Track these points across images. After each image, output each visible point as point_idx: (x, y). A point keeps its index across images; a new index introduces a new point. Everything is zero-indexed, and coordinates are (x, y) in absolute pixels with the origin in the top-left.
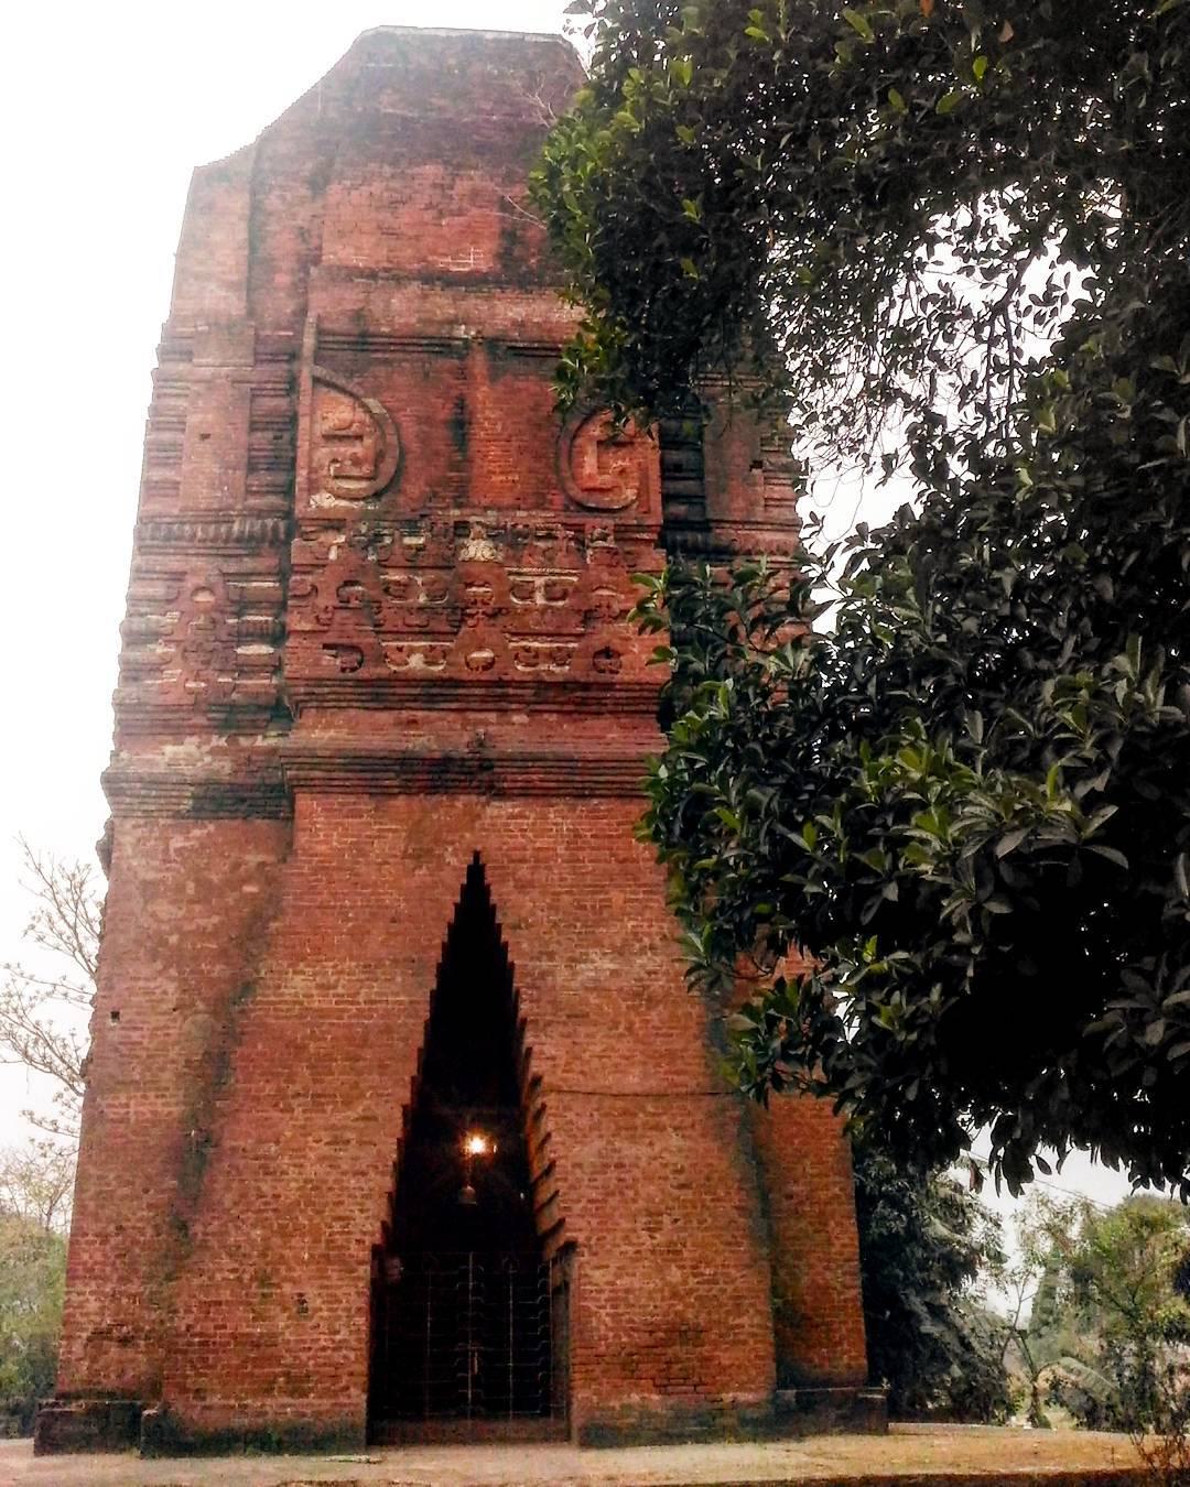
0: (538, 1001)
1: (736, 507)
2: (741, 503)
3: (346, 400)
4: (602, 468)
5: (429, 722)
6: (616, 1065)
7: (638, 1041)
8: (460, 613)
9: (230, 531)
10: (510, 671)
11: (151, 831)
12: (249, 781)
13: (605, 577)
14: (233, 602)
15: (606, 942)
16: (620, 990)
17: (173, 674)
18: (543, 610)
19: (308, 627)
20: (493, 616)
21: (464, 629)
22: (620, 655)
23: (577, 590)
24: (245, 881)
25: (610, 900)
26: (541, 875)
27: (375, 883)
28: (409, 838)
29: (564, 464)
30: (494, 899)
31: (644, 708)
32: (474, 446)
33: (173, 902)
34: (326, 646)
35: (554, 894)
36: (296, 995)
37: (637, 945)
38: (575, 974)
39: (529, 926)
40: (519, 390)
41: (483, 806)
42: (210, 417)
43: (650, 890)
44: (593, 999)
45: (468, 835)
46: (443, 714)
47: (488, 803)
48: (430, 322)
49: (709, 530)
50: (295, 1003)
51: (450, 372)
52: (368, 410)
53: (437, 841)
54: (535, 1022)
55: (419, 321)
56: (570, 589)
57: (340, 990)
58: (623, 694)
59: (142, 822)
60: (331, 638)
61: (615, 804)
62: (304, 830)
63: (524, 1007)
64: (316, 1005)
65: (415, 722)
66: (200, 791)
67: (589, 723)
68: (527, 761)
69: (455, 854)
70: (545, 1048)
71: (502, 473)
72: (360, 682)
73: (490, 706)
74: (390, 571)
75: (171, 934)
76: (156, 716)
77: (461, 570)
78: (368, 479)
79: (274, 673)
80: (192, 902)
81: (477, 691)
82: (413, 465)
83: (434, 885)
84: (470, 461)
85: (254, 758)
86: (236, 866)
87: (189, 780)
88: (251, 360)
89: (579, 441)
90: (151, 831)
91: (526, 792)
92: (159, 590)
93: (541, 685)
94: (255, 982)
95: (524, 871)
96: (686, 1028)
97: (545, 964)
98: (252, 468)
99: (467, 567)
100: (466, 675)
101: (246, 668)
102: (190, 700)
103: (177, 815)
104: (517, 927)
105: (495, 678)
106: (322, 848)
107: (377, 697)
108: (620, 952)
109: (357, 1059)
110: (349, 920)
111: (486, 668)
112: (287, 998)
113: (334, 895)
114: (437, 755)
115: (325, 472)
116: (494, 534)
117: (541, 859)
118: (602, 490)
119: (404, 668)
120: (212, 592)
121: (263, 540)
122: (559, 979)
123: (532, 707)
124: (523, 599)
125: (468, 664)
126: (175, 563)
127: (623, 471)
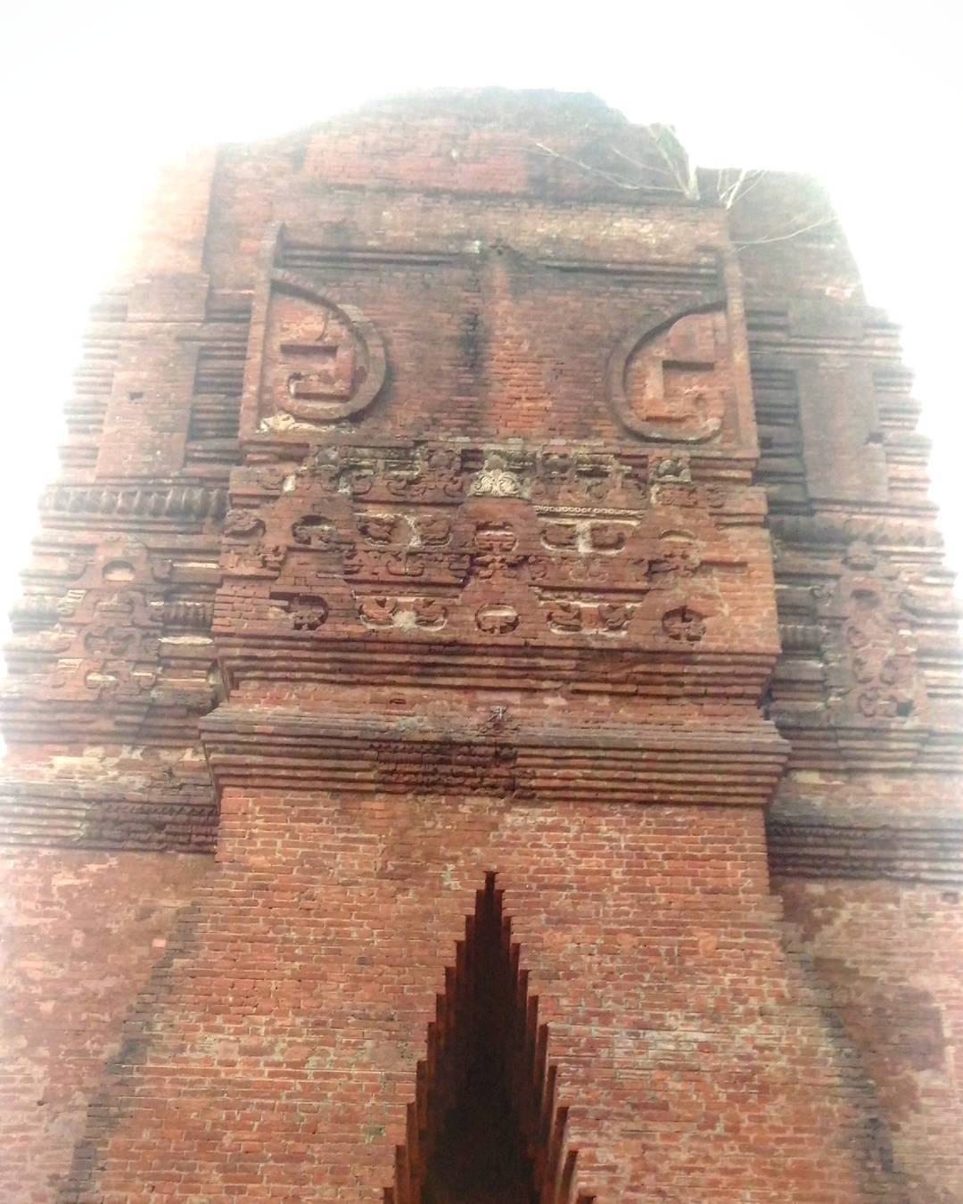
0: (585, 1081)
1: (851, 487)
2: (855, 480)
3: (317, 310)
4: (669, 395)
5: (424, 701)
6: (715, 1183)
7: (746, 1147)
8: (472, 564)
9: (160, 503)
10: (541, 634)
11: (27, 864)
12: (166, 798)
13: (679, 520)
14: (157, 579)
15: (692, 1001)
16: (716, 1070)
17: (73, 662)
18: (590, 559)
19: (249, 570)
20: (512, 566)
21: (473, 581)
22: (701, 617)
23: (636, 535)
24: (158, 933)
25: (695, 944)
26: (587, 907)
27: (337, 909)
28: (389, 851)
29: (616, 387)
30: (516, 937)
31: (738, 690)
32: (493, 368)
33: (51, 958)
34: (274, 596)
35: (608, 932)
36: (207, 1060)
37: (741, 1008)
38: (643, 1046)
39: (570, 975)
40: (555, 306)
41: (502, 811)
42: (144, 375)
43: (753, 930)
44: (675, 1085)
45: (477, 850)
46: (440, 693)
47: (507, 810)
48: (435, 236)
49: (812, 513)
50: (205, 1073)
51: (459, 284)
52: (344, 319)
53: (429, 856)
54: (581, 1114)
55: (419, 234)
56: (628, 534)
57: (277, 1057)
58: (708, 669)
59: (15, 851)
60: (282, 586)
61: (693, 815)
62: (232, 835)
63: (563, 1091)
64: (239, 1076)
65: (400, 702)
66: (98, 811)
67: (657, 708)
68: (561, 750)
69: (458, 874)
70: (599, 1153)
71: (528, 399)
72: (323, 643)
73: (512, 683)
74: (369, 507)
75: (43, 1000)
76: (44, 717)
77: (470, 507)
78: (343, 398)
79: (210, 670)
80: (76, 956)
81: (493, 661)
82: (402, 385)
83: (428, 916)
84: (485, 384)
85: (178, 773)
86: (145, 914)
87: (83, 794)
88: (201, 316)
89: (637, 364)
90: (27, 864)
91: (564, 795)
92: (61, 566)
93: (586, 654)
94: (147, 1041)
95: (562, 901)
96: (825, 1131)
97: (595, 1030)
98: (195, 434)
99: (481, 504)
100: (475, 637)
101: (165, 661)
102: (90, 696)
103: (65, 844)
104: (550, 976)
105: (521, 642)
106: (259, 860)
107: (347, 667)
108: (713, 1016)
109: (298, 1158)
110: (294, 959)
111: (503, 630)
112: (193, 1066)
113: (273, 924)
114: (433, 737)
115: (282, 388)
116: (520, 466)
117: (589, 887)
118: (669, 420)
119: (388, 627)
120: (132, 569)
121: (203, 514)
122: (619, 1053)
123: (572, 686)
124: (560, 545)
125: (479, 625)
126: (85, 537)
127: (699, 399)
